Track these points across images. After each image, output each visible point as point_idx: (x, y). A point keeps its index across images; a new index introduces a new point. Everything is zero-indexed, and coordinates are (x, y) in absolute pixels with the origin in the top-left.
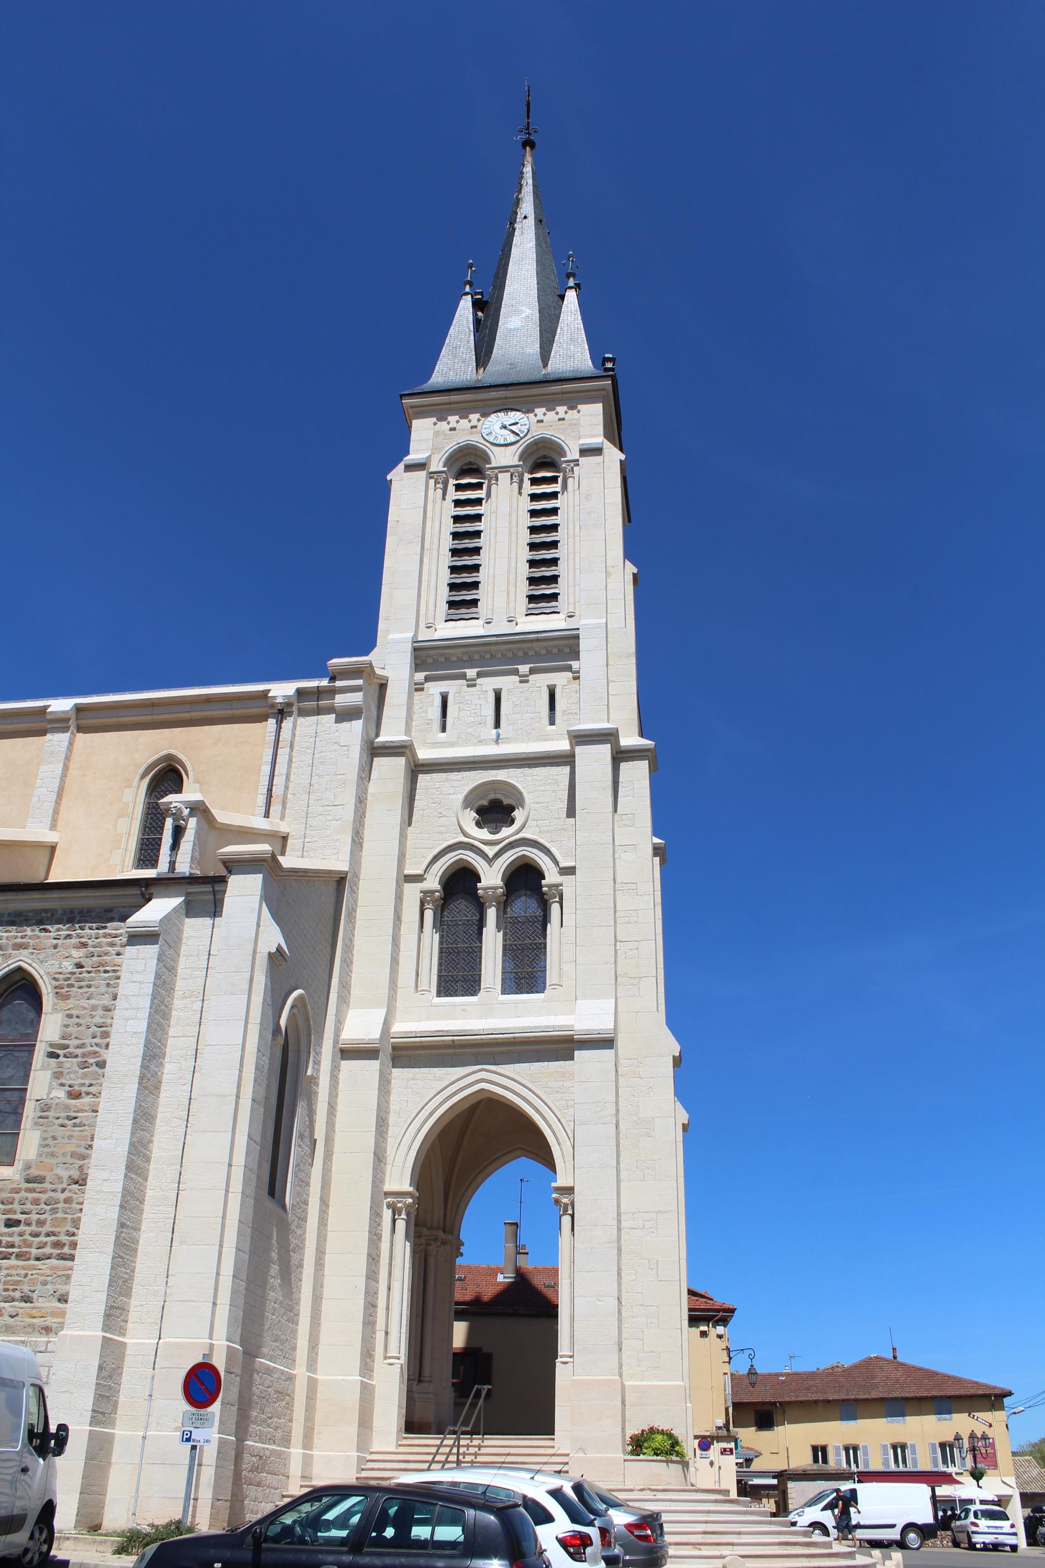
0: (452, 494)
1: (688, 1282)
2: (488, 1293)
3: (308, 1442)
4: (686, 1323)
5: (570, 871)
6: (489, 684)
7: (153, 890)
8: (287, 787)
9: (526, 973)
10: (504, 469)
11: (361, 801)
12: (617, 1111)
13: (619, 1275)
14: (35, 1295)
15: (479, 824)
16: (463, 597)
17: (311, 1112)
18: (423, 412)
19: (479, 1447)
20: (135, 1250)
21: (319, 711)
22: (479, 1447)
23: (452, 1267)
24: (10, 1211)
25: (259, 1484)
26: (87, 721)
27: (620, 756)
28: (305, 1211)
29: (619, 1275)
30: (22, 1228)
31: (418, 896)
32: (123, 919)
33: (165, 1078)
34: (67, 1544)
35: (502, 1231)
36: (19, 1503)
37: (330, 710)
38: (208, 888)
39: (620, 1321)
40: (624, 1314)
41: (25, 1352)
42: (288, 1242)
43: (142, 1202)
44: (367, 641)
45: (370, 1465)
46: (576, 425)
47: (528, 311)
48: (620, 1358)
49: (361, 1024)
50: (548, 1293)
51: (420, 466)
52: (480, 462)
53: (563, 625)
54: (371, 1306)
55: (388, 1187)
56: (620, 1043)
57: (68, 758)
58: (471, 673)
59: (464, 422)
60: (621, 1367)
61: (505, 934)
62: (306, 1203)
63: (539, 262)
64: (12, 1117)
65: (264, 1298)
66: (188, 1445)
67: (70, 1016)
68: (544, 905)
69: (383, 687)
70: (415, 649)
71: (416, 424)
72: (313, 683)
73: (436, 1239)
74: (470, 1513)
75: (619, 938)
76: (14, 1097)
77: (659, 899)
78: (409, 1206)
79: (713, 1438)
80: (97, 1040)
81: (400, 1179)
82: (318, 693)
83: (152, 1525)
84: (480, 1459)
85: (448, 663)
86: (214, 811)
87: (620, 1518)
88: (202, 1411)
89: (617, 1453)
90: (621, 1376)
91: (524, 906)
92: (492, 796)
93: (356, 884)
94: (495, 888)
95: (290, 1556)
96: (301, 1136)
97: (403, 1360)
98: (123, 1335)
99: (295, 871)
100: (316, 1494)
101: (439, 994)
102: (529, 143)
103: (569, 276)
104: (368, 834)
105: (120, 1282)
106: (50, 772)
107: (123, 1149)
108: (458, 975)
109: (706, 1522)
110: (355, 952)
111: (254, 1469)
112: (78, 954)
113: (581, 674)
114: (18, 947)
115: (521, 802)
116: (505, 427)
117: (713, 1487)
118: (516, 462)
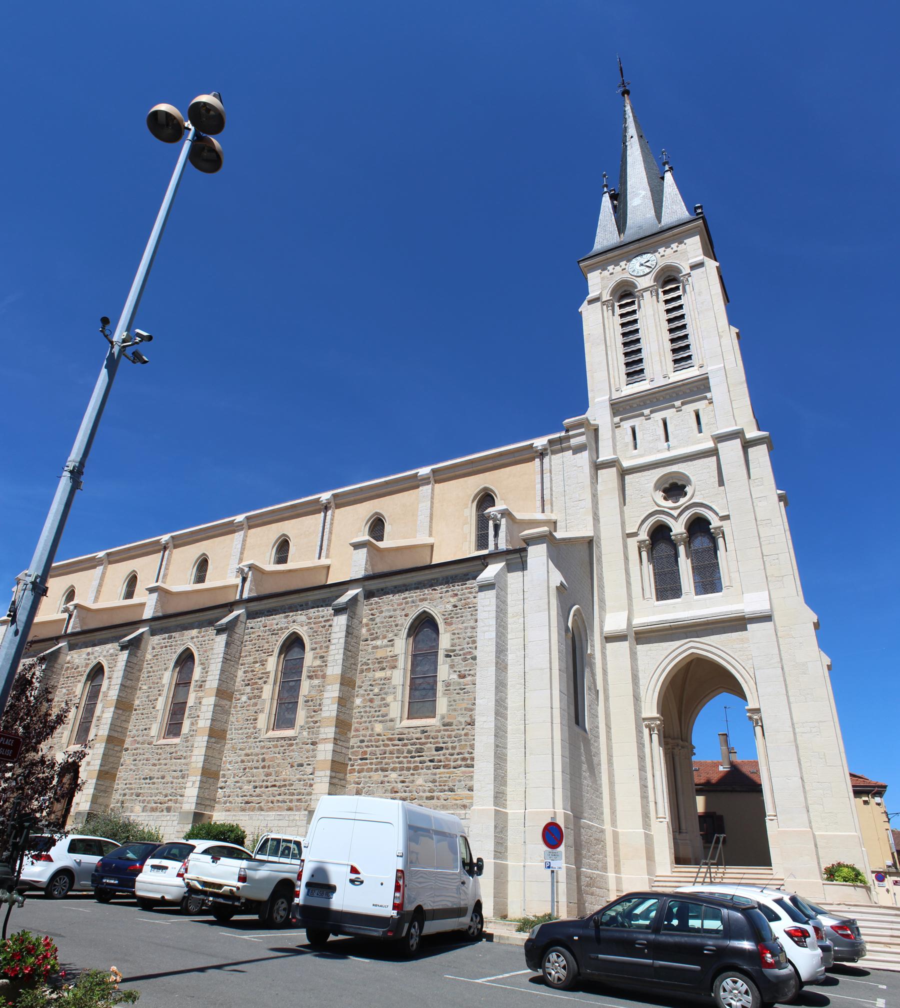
0: (618, 311)
1: (849, 769)
2: (715, 778)
3: (617, 870)
4: (852, 794)
5: (727, 518)
6: (658, 416)
7: (488, 560)
8: (551, 495)
9: (709, 580)
10: (646, 290)
11: (595, 496)
12: (781, 659)
13: (799, 762)
14: (455, 788)
15: (665, 499)
16: (634, 368)
17: (593, 675)
18: (592, 269)
19: (724, 873)
20: (506, 760)
21: (563, 450)
22: (724, 873)
23: (690, 763)
24: (436, 743)
25: (592, 894)
26: (439, 477)
27: (747, 445)
28: (598, 732)
29: (799, 762)
30: (444, 751)
31: (637, 544)
32: (475, 578)
33: (509, 662)
34: (490, 925)
35: (718, 740)
36: (462, 903)
37: (569, 448)
38: (518, 555)
39: (805, 792)
40: (807, 788)
41: (455, 818)
42: (590, 751)
43: (506, 732)
44: (582, 405)
45: (656, 884)
46: (685, 252)
47: (643, 193)
48: (809, 817)
49: (614, 620)
50: (754, 777)
51: (597, 299)
52: (630, 289)
53: (698, 373)
54: (644, 787)
55: (644, 715)
56: (776, 617)
57: (432, 498)
58: (647, 412)
59: (618, 268)
60: (810, 823)
61: (692, 560)
62: (597, 727)
63: (645, 161)
64: (431, 692)
65: (581, 784)
66: (549, 871)
67: (454, 634)
68: (714, 540)
69: (596, 430)
70: (612, 405)
71: (589, 276)
72: (557, 435)
73: (678, 745)
74: (725, 911)
75: (765, 554)
76: (431, 680)
77: (787, 527)
78: (658, 726)
79: (886, 873)
80: (470, 645)
81: (651, 710)
82: (560, 440)
83: (535, 916)
84: (725, 881)
85: (632, 409)
86: (515, 514)
87: (827, 922)
88: (554, 850)
89: (817, 879)
90: (811, 828)
91: (701, 542)
92: (671, 481)
93: (599, 543)
94: (681, 534)
95: (617, 934)
96: (589, 689)
97: (668, 819)
98: (506, 808)
99: (564, 540)
100: (628, 898)
101: (658, 600)
102: (626, 92)
103: (664, 164)
104: (601, 513)
105: (500, 778)
106: (424, 507)
107: (492, 704)
108: (667, 587)
109: (891, 929)
110: (605, 580)
111: (588, 885)
112: (453, 600)
113: (714, 400)
114: (422, 600)
115: (689, 482)
116: (642, 265)
117: (891, 905)
118: (653, 284)
